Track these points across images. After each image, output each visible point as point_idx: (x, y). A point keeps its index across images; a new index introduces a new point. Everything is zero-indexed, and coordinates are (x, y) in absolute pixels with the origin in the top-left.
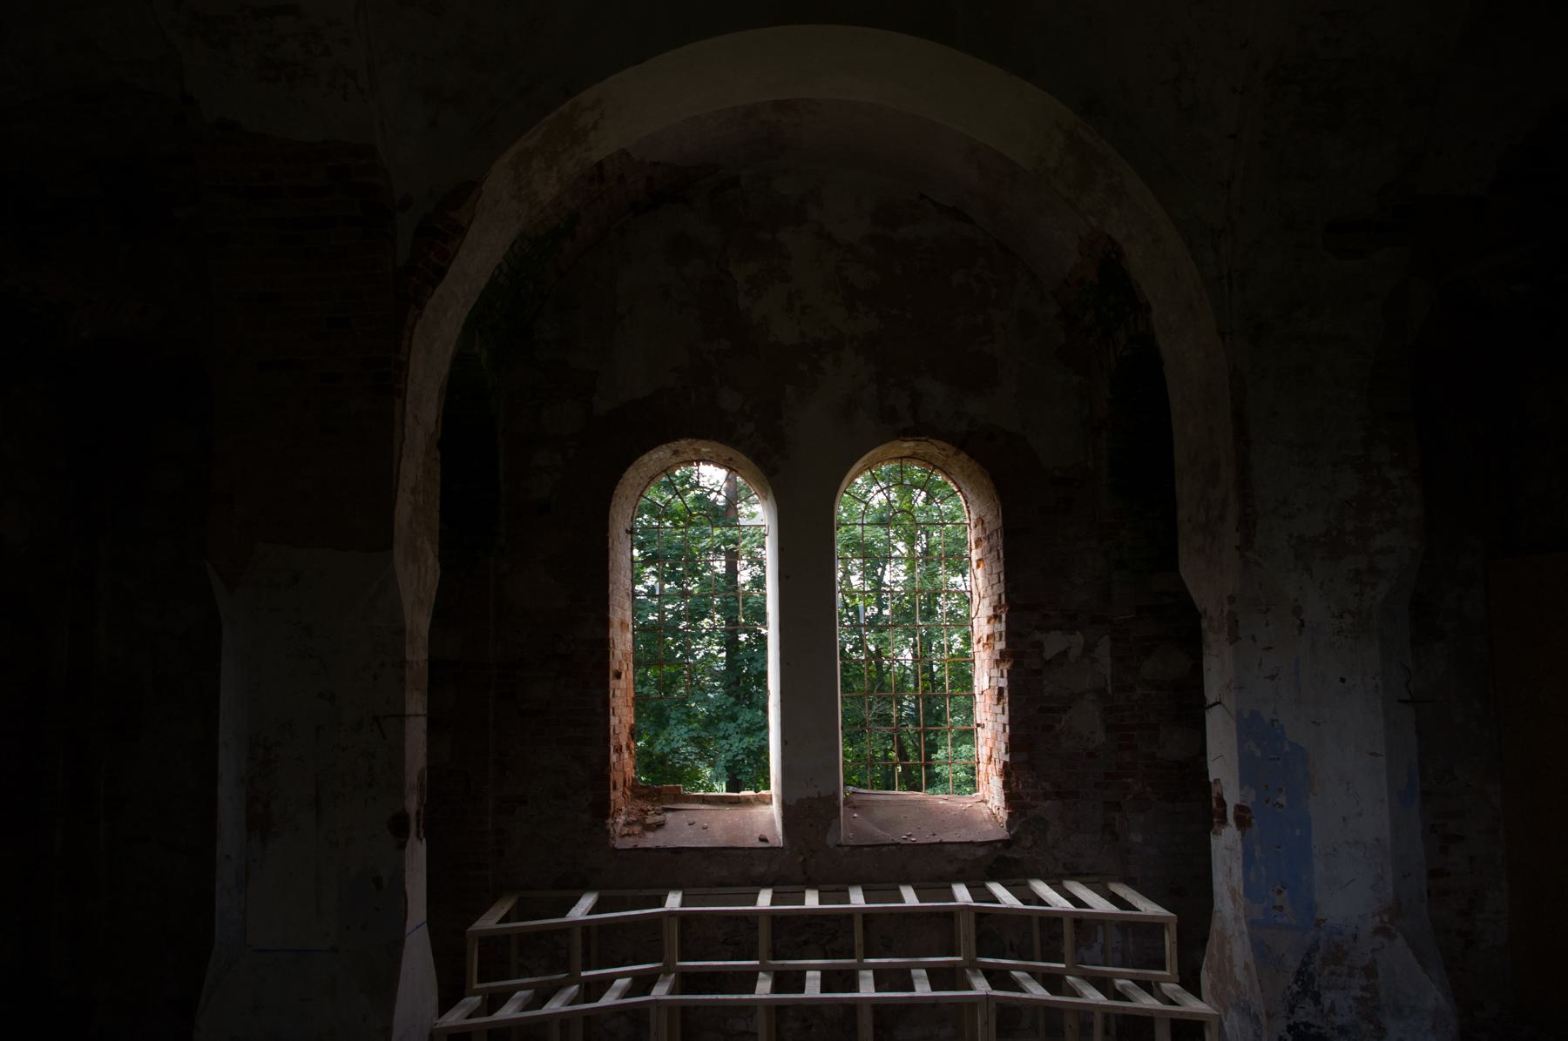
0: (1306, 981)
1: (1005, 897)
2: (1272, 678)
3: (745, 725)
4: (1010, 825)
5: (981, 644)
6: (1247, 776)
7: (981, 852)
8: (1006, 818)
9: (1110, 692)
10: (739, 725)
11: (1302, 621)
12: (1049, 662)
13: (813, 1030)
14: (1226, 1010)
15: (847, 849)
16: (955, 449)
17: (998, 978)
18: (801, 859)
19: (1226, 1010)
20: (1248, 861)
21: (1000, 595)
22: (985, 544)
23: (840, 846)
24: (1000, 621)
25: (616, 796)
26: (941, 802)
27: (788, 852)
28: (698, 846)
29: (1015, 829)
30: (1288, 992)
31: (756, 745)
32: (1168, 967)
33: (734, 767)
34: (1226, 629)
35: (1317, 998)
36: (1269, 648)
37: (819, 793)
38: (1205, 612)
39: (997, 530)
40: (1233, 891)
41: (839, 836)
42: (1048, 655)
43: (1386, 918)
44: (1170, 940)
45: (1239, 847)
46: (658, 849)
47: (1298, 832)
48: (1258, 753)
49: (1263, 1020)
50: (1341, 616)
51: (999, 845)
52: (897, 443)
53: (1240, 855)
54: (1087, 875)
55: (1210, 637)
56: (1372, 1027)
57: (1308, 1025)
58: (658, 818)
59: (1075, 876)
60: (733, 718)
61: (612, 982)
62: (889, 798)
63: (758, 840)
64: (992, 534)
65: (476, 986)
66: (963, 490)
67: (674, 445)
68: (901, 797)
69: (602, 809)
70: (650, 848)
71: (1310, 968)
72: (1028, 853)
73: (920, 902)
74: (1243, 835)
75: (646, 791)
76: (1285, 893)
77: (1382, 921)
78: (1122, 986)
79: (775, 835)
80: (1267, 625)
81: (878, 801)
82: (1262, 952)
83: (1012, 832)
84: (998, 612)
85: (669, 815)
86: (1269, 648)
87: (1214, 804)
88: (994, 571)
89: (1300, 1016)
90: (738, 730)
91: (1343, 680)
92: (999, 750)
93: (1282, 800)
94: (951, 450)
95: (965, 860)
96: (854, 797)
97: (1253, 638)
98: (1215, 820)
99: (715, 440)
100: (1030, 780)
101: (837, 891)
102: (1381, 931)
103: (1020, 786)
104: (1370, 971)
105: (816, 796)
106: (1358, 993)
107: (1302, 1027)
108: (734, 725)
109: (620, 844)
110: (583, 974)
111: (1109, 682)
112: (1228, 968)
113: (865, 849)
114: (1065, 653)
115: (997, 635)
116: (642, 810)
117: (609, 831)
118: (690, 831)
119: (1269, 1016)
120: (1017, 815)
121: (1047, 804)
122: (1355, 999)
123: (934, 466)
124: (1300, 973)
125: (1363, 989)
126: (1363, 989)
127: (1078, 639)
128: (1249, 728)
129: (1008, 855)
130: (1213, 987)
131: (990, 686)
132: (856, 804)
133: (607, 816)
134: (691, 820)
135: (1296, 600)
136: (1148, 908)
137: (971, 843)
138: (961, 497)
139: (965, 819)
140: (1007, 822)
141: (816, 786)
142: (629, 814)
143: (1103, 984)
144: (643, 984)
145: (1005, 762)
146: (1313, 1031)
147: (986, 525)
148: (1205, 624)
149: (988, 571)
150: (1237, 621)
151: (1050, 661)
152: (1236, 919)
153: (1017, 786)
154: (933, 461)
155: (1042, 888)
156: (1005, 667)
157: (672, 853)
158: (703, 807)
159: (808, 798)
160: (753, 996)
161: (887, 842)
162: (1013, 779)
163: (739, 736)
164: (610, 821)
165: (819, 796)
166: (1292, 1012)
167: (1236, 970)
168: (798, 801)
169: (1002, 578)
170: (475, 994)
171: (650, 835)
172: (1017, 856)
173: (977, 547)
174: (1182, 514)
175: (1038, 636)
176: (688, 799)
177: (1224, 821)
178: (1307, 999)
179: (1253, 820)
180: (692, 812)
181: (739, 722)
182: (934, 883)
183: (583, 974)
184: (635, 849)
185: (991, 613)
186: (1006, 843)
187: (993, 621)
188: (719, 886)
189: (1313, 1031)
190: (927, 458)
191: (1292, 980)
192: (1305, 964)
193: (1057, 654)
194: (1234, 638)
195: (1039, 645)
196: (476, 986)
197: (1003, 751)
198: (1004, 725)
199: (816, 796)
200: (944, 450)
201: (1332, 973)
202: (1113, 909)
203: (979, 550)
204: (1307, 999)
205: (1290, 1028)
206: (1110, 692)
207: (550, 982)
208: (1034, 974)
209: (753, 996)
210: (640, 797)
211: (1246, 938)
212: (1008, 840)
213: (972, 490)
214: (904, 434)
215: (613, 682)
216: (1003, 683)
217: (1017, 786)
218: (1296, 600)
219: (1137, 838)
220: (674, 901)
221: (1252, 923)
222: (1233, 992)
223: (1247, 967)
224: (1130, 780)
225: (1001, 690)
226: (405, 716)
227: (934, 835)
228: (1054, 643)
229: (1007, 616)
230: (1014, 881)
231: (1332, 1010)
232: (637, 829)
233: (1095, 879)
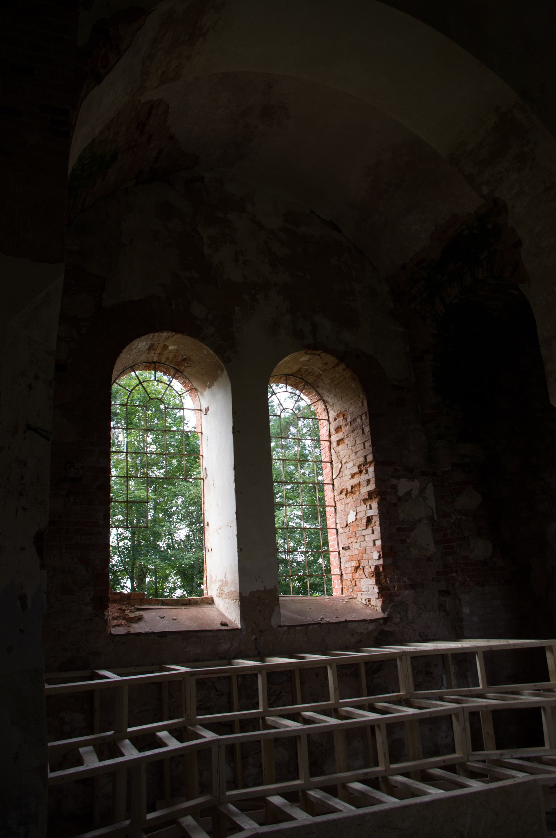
4: (384, 609)
7: (371, 627)
9: (436, 519)
15: (285, 628)
18: (254, 637)
23: (280, 626)
26: (327, 600)
27: (244, 633)
28: (178, 630)
29: (389, 610)
37: (265, 587)
39: (361, 416)
46: (147, 634)
51: (382, 621)
58: (137, 613)
63: (220, 625)
70: (141, 633)
72: (398, 627)
81: (286, 600)
88: (358, 442)
95: (362, 633)
99: (188, 335)
103: (388, 582)
105: (263, 590)
109: (116, 631)
110: (129, 730)
113: (298, 628)
114: (409, 493)
120: (388, 601)
121: (407, 592)
127: (416, 484)
129: (386, 629)
131: (356, 519)
134: (162, 615)
137: (365, 621)
138: (282, 427)
141: (262, 582)
145: (377, 567)
153: (386, 581)
157: (158, 637)
158: (164, 607)
159: (258, 591)
160: (81, 769)
161: (312, 622)
165: (265, 589)
168: (250, 593)
171: (135, 625)
172: (391, 630)
175: (394, 481)
180: (161, 610)
183: (129, 730)
184: (129, 634)
186: (385, 620)
188: (195, 662)
193: (405, 493)
195: (395, 487)
199: (263, 590)
209: (81, 769)
213: (335, 395)
227: (337, 617)
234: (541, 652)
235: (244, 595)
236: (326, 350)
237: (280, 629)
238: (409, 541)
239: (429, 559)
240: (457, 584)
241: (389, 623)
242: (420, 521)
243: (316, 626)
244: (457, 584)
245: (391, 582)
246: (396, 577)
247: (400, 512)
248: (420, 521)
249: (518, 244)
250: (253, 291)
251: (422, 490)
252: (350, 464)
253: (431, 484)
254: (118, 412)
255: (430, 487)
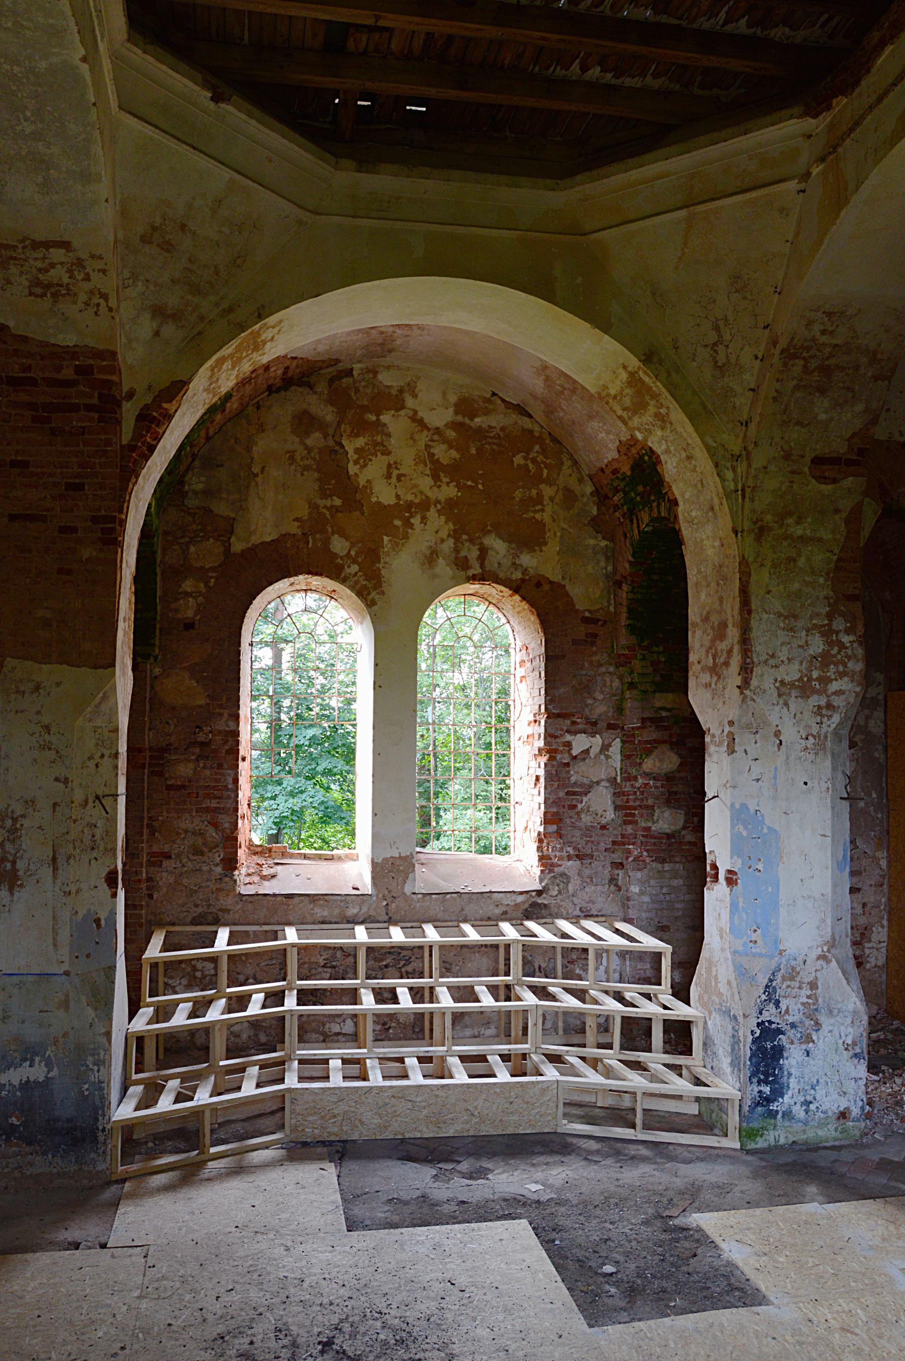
0: (771, 995)
1: (544, 935)
2: (758, 780)
3: (289, 789)
5: (522, 741)
6: (736, 850)
7: (520, 899)
8: (539, 873)
9: (619, 781)
10: (285, 789)
11: (781, 741)
12: (575, 757)
13: (391, 1031)
14: (710, 1014)
15: (420, 896)
16: (511, 592)
17: (541, 992)
18: (385, 903)
19: (710, 1014)
20: (734, 908)
21: (540, 706)
22: (528, 664)
23: (414, 893)
24: (539, 725)
25: (242, 853)
27: (375, 898)
30: (759, 1000)
31: (299, 805)
32: (663, 982)
33: (281, 822)
34: (726, 744)
35: (777, 1004)
36: (756, 759)
38: (709, 730)
40: (721, 930)
41: (414, 886)
42: (575, 752)
43: (825, 949)
44: (666, 964)
45: (728, 899)
47: (770, 889)
48: (745, 833)
49: (741, 1019)
50: (807, 739)
51: (534, 894)
52: (467, 585)
53: (728, 905)
54: (597, 916)
55: (711, 749)
56: (812, 1022)
57: (770, 1022)
58: (272, 871)
59: (588, 916)
60: (280, 783)
61: (251, 996)
62: (448, 857)
64: (535, 658)
65: (149, 1000)
66: (511, 622)
67: (292, 579)
68: (457, 857)
69: (231, 863)
71: (774, 984)
73: (406, 937)
74: (731, 890)
75: (259, 849)
76: (759, 931)
77: (823, 951)
78: (631, 997)
79: (364, 885)
80: (756, 742)
81: (440, 860)
82: (742, 973)
83: (543, 884)
84: (538, 718)
85: (279, 867)
86: (756, 759)
87: (708, 868)
88: (536, 687)
89: (766, 1016)
90: (284, 793)
91: (806, 783)
92: (534, 823)
93: (760, 867)
94: (507, 592)
96: (419, 855)
97: (745, 751)
98: (708, 879)
99: (327, 576)
100: (558, 846)
101: (412, 927)
102: (822, 957)
104: (813, 985)
105: (397, 856)
106: (805, 1000)
107: (767, 1024)
108: (279, 788)
109: (244, 890)
111: (619, 773)
112: (713, 984)
114: (587, 752)
115: (536, 737)
116: (258, 864)
117: (235, 881)
118: (298, 880)
119: (745, 1016)
122: (803, 1004)
123: (490, 603)
124: (767, 986)
125: (808, 997)
126: (808, 997)
127: (598, 740)
128: (739, 815)
129: (540, 902)
130: (700, 997)
132: (424, 861)
133: (236, 868)
135: (777, 726)
136: (649, 942)
139: (507, 874)
140: (540, 877)
142: (248, 867)
143: (619, 997)
144: (276, 998)
145: (539, 834)
146: (774, 1026)
147: (530, 651)
148: (707, 739)
149: (531, 686)
150: (734, 739)
151: (576, 757)
152: (723, 950)
153: (548, 850)
154: (489, 599)
155: (565, 925)
156: (543, 760)
159: (392, 857)
162: (545, 844)
163: (285, 798)
164: (236, 873)
166: (761, 1013)
167: (720, 985)
169: (543, 692)
170: (148, 1005)
171: (266, 883)
172: (546, 902)
173: (520, 666)
174: (693, 658)
175: (568, 737)
176: (292, 856)
177: (716, 878)
178: (771, 1005)
179: (739, 881)
181: (284, 786)
182: (487, 922)
185: (532, 718)
186: (539, 893)
187: (533, 724)
189: (774, 1026)
190: (485, 596)
191: (762, 991)
192: (771, 981)
194: (731, 751)
195: (569, 744)
196: (149, 1000)
197: (539, 823)
198: (540, 804)
200: (501, 592)
201: (788, 987)
202: (624, 942)
203: (523, 669)
204: (771, 1005)
205: (758, 1025)
206: (619, 781)
207: (204, 997)
208: (567, 990)
210: (255, 853)
211: (730, 962)
212: (540, 891)
214: (474, 579)
215: (241, 764)
216: (541, 772)
217: (548, 850)
218: (777, 726)
219: (635, 889)
220: (291, 935)
221: (735, 953)
222: (717, 1000)
223: (729, 983)
224: (631, 847)
225: (538, 778)
226: (118, 795)
228: (580, 743)
229: (546, 722)
230: (544, 921)
231: (787, 1011)
232: (256, 879)
233: (603, 919)
234: (298, 1005)
235: (376, 861)
236: (497, 580)
237: (414, 896)
238: (580, 806)
239: (603, 827)
240: (631, 859)
241: (544, 895)
242: (598, 783)
243: (455, 895)
244: (631, 859)
245: (553, 851)
246: (558, 846)
247: (572, 772)
248: (598, 783)
249: (676, 503)
250: (407, 514)
251: (605, 747)
252: (528, 709)
253: (618, 740)
254: (446, 476)
255: (617, 745)
